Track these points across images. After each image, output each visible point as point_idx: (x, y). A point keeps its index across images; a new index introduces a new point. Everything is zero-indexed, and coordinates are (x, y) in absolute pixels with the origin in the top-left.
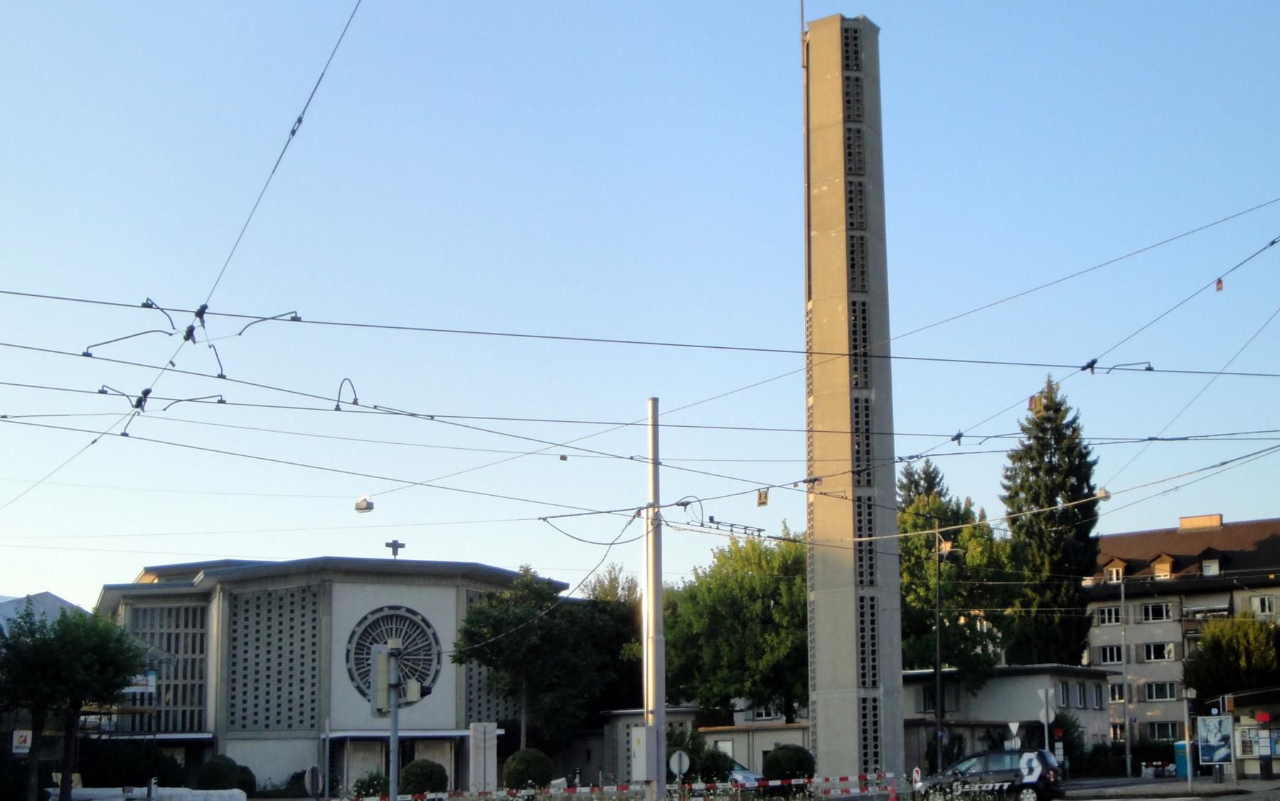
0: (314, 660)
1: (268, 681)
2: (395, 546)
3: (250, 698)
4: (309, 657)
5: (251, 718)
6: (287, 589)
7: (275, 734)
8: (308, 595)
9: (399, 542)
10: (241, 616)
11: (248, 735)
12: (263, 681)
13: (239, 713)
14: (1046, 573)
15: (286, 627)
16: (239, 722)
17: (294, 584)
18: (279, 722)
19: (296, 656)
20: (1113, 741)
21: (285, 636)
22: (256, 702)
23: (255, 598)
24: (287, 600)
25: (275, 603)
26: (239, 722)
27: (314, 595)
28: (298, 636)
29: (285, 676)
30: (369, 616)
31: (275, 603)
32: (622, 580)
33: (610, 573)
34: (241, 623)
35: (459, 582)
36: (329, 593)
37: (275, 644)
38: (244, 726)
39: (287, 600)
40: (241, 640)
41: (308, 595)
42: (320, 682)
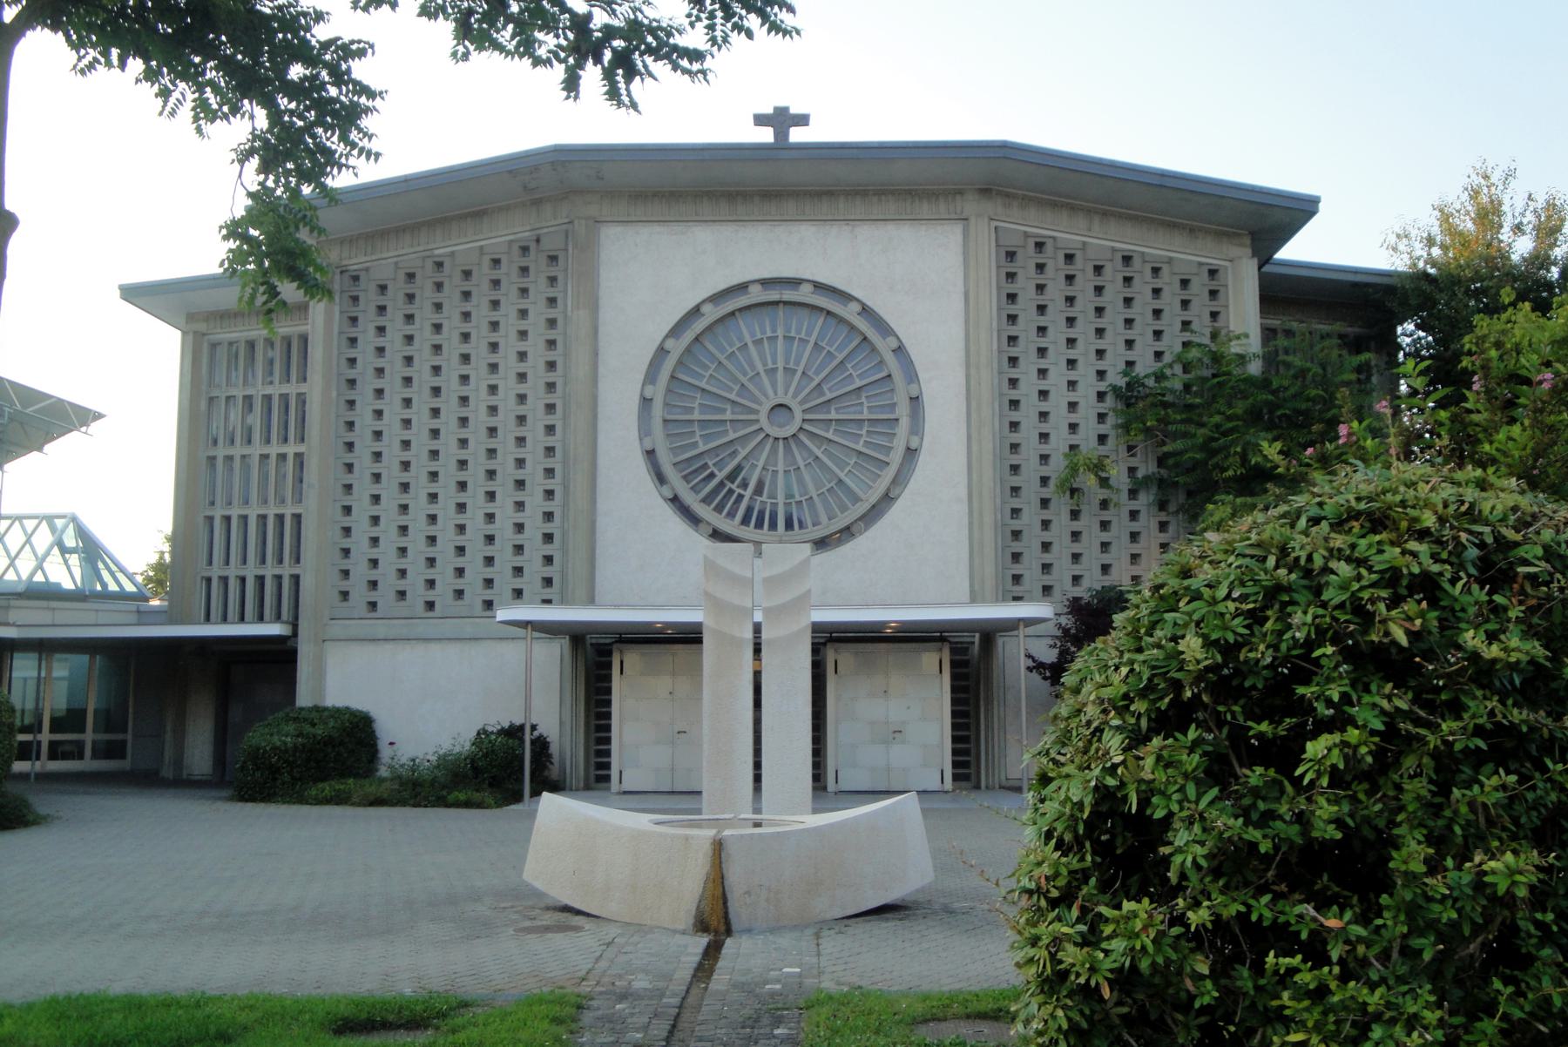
0: (550, 429)
1: (433, 488)
2: (781, 119)
3: (388, 531)
4: (537, 420)
5: (389, 583)
6: (481, 248)
7: (448, 628)
8: (536, 262)
9: (793, 111)
10: (369, 322)
11: (381, 628)
12: (421, 487)
13: (360, 572)
14: (1189, 984)
15: (478, 348)
16: (360, 594)
17: (500, 235)
18: (459, 594)
19: (505, 421)
20: (1373, 816)
21: (477, 371)
22: (489, 552)
23: (401, 276)
24: (484, 273)
25: (454, 285)
26: (360, 594)
27: (553, 259)
28: (509, 365)
29: (476, 475)
30: (706, 309)
31: (454, 285)
32: (1514, 205)
33: (1475, 194)
34: (368, 339)
35: (971, 205)
36: (590, 248)
37: (452, 388)
38: (430, 605)
39: (484, 273)
40: (368, 383)
41: (536, 262)
42: (566, 487)
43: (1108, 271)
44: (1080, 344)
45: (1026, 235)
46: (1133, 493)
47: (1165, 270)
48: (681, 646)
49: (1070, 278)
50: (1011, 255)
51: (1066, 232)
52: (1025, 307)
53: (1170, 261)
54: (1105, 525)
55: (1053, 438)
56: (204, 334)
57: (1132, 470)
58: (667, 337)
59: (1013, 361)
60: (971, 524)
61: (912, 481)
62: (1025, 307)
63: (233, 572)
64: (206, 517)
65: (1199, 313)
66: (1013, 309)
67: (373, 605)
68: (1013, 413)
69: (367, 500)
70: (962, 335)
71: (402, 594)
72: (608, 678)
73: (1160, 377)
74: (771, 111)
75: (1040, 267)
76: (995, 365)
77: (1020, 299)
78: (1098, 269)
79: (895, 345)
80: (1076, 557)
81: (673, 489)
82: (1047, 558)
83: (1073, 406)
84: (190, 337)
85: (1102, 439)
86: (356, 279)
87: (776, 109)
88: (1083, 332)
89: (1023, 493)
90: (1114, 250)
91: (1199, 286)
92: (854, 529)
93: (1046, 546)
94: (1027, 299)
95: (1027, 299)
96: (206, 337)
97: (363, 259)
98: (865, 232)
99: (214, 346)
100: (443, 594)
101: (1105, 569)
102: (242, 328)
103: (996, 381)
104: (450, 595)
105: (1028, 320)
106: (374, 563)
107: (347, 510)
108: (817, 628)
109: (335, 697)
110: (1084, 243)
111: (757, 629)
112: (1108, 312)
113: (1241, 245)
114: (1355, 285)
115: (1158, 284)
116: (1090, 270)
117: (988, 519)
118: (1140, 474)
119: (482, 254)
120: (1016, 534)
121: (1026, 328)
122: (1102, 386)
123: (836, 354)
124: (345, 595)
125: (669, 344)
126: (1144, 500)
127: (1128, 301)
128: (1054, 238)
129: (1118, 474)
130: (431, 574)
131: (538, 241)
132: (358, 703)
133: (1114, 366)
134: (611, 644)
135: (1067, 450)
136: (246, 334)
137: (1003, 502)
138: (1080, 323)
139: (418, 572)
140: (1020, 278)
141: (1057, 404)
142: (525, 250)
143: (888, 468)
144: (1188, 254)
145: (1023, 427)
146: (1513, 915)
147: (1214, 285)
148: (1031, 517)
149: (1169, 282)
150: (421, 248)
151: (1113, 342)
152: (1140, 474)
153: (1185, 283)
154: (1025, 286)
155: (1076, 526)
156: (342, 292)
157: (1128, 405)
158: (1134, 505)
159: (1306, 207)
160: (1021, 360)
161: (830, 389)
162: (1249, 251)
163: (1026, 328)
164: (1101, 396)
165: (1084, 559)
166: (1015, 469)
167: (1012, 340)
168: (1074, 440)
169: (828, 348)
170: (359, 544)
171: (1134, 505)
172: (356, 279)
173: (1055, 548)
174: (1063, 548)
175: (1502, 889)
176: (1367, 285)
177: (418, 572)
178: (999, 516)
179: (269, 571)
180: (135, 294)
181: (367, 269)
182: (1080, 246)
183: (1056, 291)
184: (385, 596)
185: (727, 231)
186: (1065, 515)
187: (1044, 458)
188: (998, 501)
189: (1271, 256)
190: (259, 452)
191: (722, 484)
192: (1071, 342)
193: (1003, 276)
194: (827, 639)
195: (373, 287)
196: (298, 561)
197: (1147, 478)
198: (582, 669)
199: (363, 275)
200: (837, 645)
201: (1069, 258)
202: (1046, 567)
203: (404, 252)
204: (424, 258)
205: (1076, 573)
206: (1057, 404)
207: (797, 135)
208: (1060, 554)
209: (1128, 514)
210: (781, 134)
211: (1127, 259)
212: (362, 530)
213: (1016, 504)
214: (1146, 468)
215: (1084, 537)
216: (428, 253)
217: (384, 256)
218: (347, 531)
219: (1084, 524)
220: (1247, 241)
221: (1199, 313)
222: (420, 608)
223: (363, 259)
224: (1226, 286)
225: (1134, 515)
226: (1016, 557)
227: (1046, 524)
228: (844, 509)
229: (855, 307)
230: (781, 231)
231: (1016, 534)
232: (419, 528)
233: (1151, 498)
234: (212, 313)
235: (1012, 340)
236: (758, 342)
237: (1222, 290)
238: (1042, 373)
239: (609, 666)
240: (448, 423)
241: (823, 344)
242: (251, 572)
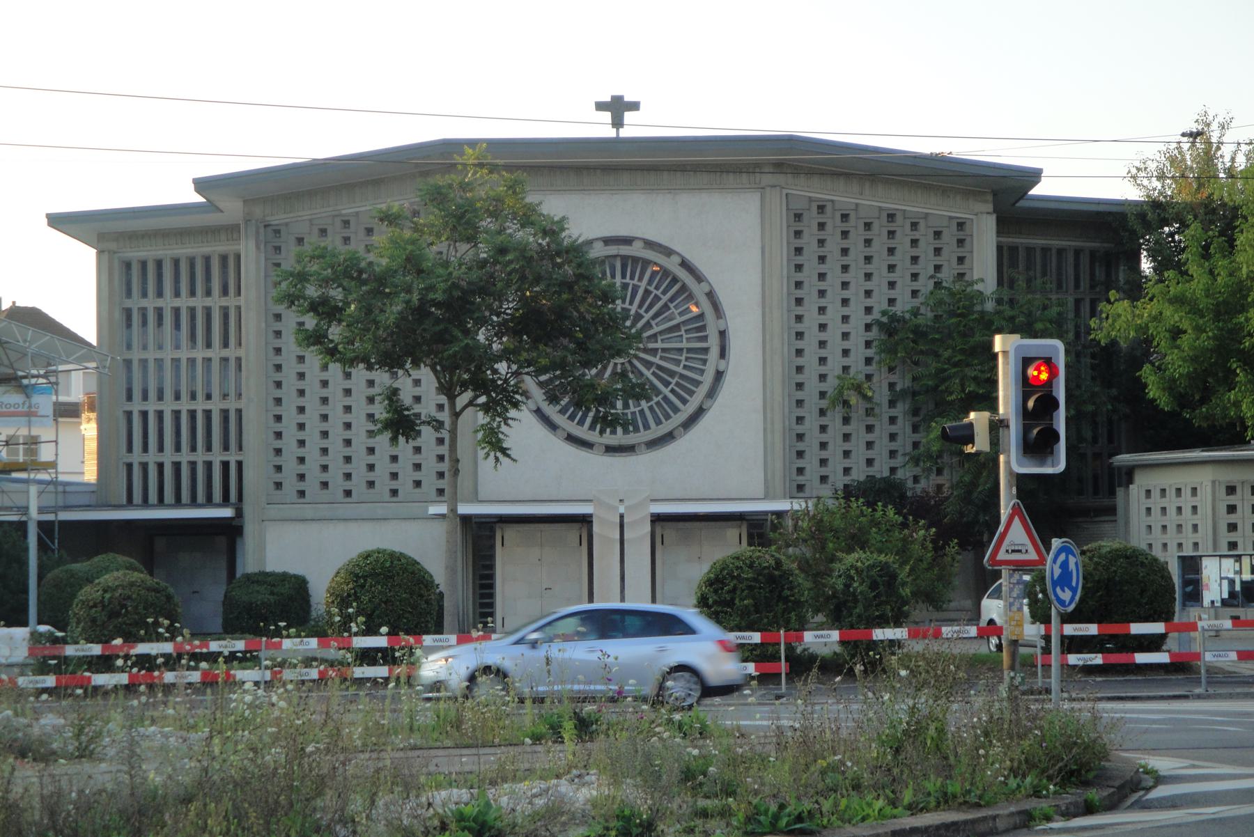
2: (618, 108)
7: (363, 509)
9: (626, 99)
11: (308, 511)
13: (291, 467)
16: (291, 485)
18: (418, 484)
26: (291, 485)
38: (348, 493)
43: (876, 226)
44: (852, 286)
45: (811, 200)
46: (892, 403)
47: (922, 226)
48: (547, 525)
49: (845, 234)
50: (798, 217)
51: (842, 196)
52: (809, 258)
54: (870, 429)
55: (829, 361)
56: (115, 253)
57: (892, 386)
59: (799, 301)
60: (765, 430)
61: (720, 395)
62: (809, 258)
63: (152, 457)
64: (125, 412)
65: (948, 259)
66: (799, 260)
67: (302, 493)
68: (798, 342)
69: (294, 410)
70: (760, 282)
71: (325, 485)
72: (493, 547)
73: (915, 312)
74: (609, 99)
75: (822, 226)
76: (785, 305)
77: (805, 252)
78: (868, 226)
79: (707, 289)
80: (847, 454)
81: (536, 403)
82: (824, 454)
83: (845, 336)
84: (106, 256)
85: (868, 361)
86: (277, 232)
87: (613, 97)
88: (856, 276)
89: (806, 404)
90: (880, 209)
91: (949, 238)
92: (676, 433)
93: (823, 445)
94: (811, 251)
95: (811, 251)
96: (116, 255)
99: (128, 265)
100: (358, 484)
101: (870, 462)
102: (149, 248)
103: (785, 316)
104: (364, 485)
105: (811, 269)
106: (302, 460)
107: (278, 418)
108: (653, 515)
109: (274, 565)
110: (857, 205)
111: (622, 516)
112: (875, 260)
113: (986, 201)
114: (1098, 213)
115: (916, 235)
116: (861, 227)
117: (778, 426)
118: (898, 388)
120: (800, 437)
121: (809, 275)
122: (869, 319)
123: (662, 296)
124: (278, 485)
126: (900, 409)
127: (891, 251)
128: (832, 201)
129: (880, 393)
130: (348, 468)
132: (293, 569)
133: (879, 303)
134: (495, 523)
135: (840, 372)
136: (153, 253)
137: (790, 412)
138: (852, 269)
139: (337, 468)
140: (806, 235)
141: (833, 336)
143: (701, 386)
144: (941, 210)
145: (806, 353)
147: (961, 235)
148: (812, 424)
150: (331, 209)
151: (879, 284)
152: (898, 388)
153: (938, 234)
154: (809, 241)
155: (847, 429)
156: (266, 243)
157: (890, 335)
158: (893, 412)
160: (805, 300)
161: (662, 340)
162: (990, 207)
163: (809, 275)
164: (868, 327)
165: (853, 455)
166: (800, 386)
167: (799, 285)
168: (846, 361)
169: (655, 292)
170: (289, 443)
171: (893, 412)
172: (277, 232)
173: (831, 447)
174: (836, 447)
175: (386, 402)
176: (1110, 213)
177: (337, 468)
178: (787, 423)
179: (185, 457)
180: (59, 222)
181: (287, 224)
182: (853, 207)
183: (834, 245)
184: (311, 486)
186: (839, 420)
187: (823, 377)
188: (787, 410)
189: (1026, 193)
190: (170, 357)
192: (845, 285)
193: (792, 234)
194: (657, 519)
196: (240, 448)
197: (903, 390)
198: (470, 542)
199: (283, 229)
200: (664, 523)
201: (845, 217)
202: (823, 462)
203: (315, 211)
204: (334, 216)
205: (847, 466)
206: (833, 336)
207: (636, 127)
208: (834, 453)
209: (887, 419)
210: (618, 123)
211: (891, 217)
212: (291, 435)
213: (800, 412)
214: (903, 382)
215: (853, 438)
216: (337, 213)
217: (300, 214)
218: (279, 435)
219: (856, 427)
220: (990, 198)
221: (948, 259)
222: (340, 495)
224: (972, 235)
225: (893, 420)
226: (800, 454)
227: (823, 429)
228: (668, 417)
229: (676, 260)
231: (800, 437)
232: (337, 433)
233: (907, 407)
234: (122, 233)
235: (799, 285)
237: (968, 240)
238: (822, 310)
239: (493, 537)
242: (168, 457)
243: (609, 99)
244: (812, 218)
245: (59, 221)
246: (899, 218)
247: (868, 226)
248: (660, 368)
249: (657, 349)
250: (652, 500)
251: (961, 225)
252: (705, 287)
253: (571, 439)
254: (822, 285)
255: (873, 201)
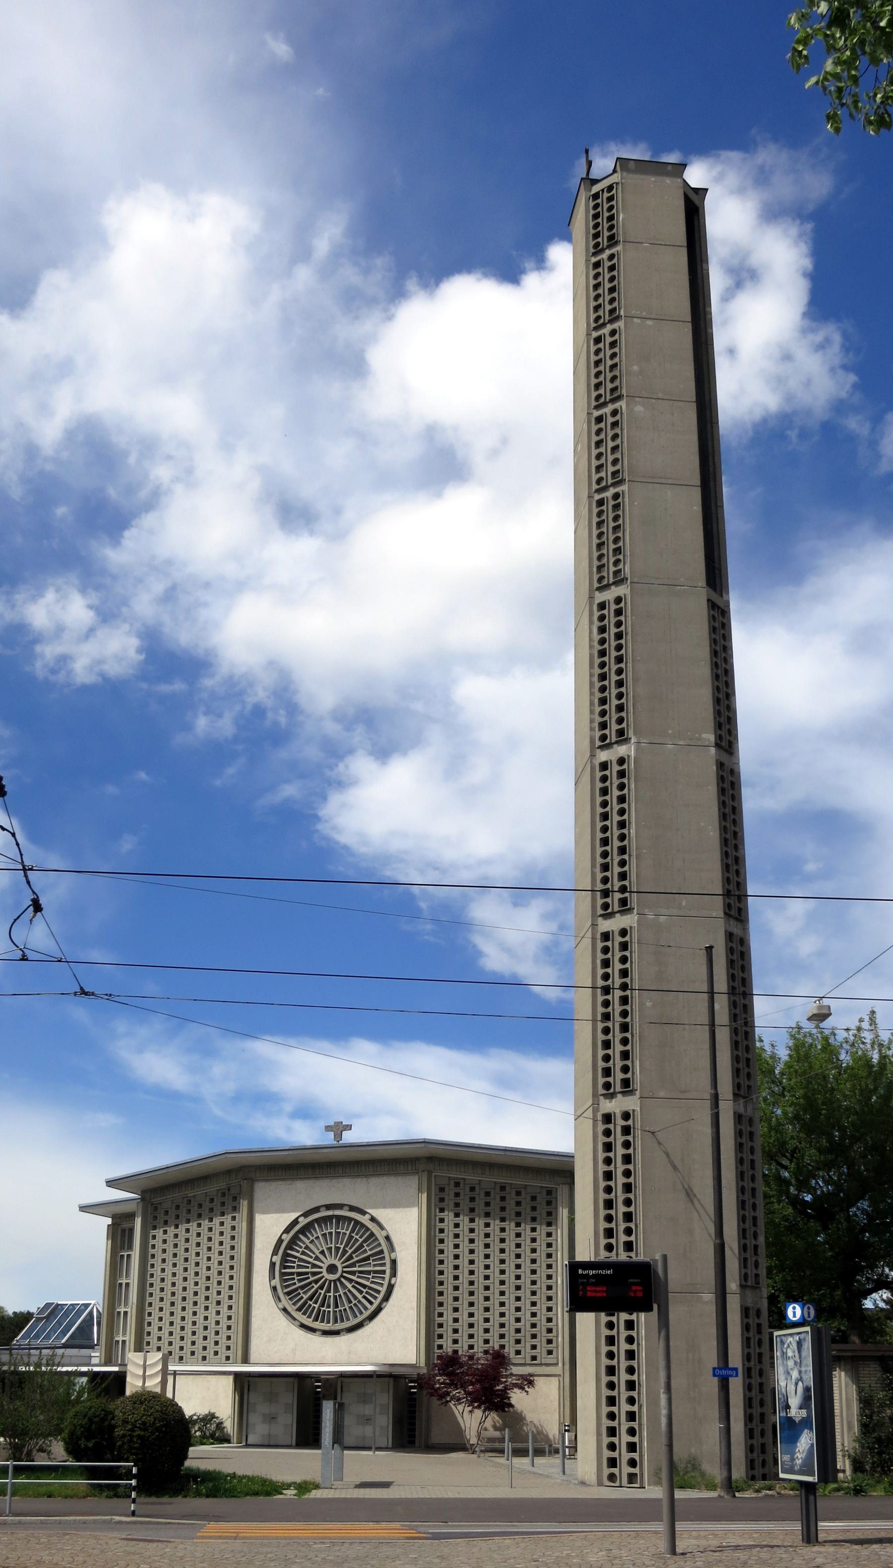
6: (206, 1193)
17: (212, 1188)
30: (301, 1219)
53: (526, 1187)
58: (283, 1233)
74: (333, 1124)
78: (488, 1194)
97: (159, 1199)
98: (374, 1181)
115: (519, 1199)
119: (206, 1196)
125: (275, 1259)
131: (229, 1190)
142: (224, 1195)
146: (465, 1391)
149: (525, 1199)
153: (534, 1198)
159: (737, 1115)
185: (310, 1183)
191: (306, 1303)
195: (162, 1212)
201: (472, 1189)
204: (183, 1198)
207: (348, 1137)
210: (338, 1136)
211: (503, 1188)
223: (159, 1199)
230: (334, 1181)
236: (312, 1242)
237: (554, 1201)
240: (527, 1278)
241: (353, 1235)
243: (333, 1124)
244: (450, 1191)
245: (84, 1208)
246: (508, 1189)
247: (488, 1194)
248: (360, 1272)
249: (347, 1287)
250: (569, 225)
251: (549, 1192)
252: (384, 1233)
253: (303, 1326)
254: (457, 1231)
255: (489, 1179)
